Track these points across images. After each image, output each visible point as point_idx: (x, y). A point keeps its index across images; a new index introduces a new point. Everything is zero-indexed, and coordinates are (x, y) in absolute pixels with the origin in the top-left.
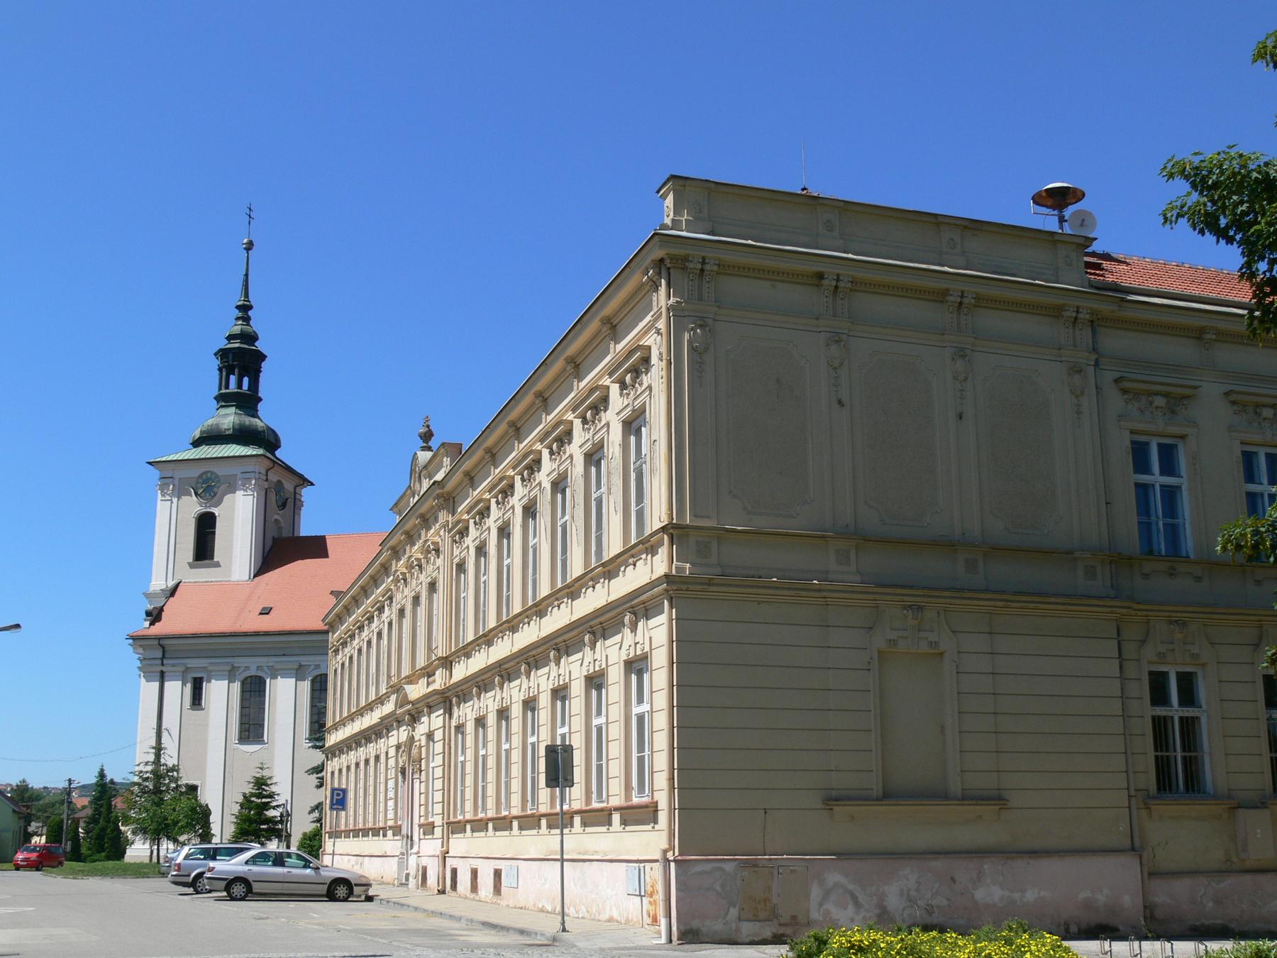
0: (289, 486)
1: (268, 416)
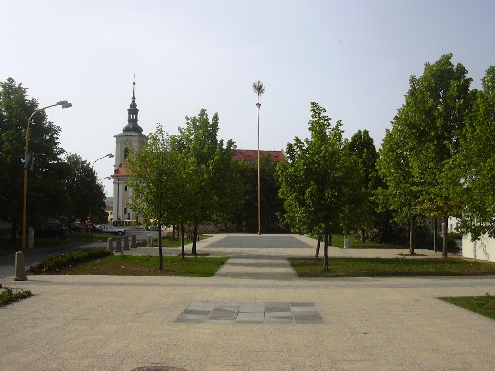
0: (145, 140)
1: (139, 123)
